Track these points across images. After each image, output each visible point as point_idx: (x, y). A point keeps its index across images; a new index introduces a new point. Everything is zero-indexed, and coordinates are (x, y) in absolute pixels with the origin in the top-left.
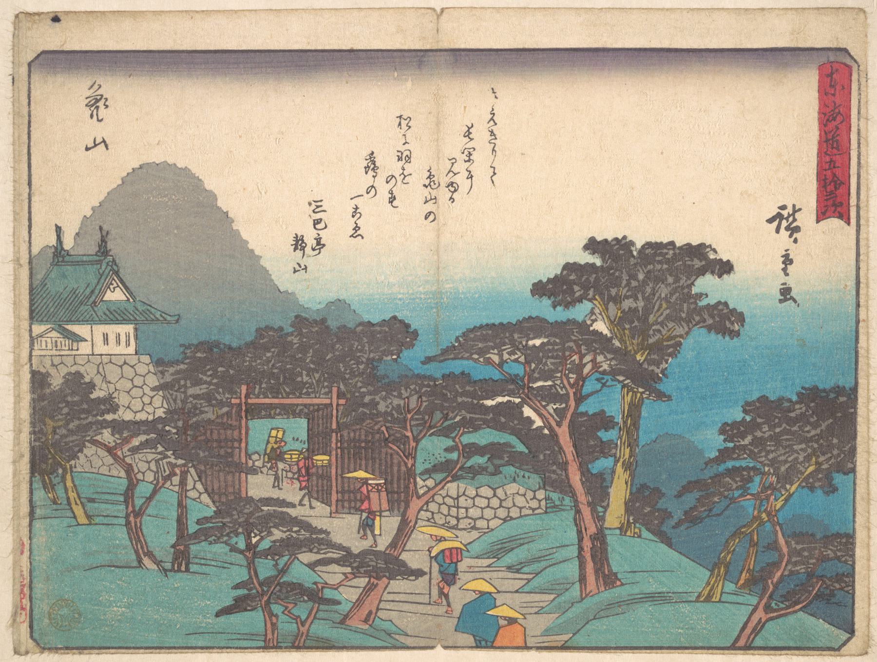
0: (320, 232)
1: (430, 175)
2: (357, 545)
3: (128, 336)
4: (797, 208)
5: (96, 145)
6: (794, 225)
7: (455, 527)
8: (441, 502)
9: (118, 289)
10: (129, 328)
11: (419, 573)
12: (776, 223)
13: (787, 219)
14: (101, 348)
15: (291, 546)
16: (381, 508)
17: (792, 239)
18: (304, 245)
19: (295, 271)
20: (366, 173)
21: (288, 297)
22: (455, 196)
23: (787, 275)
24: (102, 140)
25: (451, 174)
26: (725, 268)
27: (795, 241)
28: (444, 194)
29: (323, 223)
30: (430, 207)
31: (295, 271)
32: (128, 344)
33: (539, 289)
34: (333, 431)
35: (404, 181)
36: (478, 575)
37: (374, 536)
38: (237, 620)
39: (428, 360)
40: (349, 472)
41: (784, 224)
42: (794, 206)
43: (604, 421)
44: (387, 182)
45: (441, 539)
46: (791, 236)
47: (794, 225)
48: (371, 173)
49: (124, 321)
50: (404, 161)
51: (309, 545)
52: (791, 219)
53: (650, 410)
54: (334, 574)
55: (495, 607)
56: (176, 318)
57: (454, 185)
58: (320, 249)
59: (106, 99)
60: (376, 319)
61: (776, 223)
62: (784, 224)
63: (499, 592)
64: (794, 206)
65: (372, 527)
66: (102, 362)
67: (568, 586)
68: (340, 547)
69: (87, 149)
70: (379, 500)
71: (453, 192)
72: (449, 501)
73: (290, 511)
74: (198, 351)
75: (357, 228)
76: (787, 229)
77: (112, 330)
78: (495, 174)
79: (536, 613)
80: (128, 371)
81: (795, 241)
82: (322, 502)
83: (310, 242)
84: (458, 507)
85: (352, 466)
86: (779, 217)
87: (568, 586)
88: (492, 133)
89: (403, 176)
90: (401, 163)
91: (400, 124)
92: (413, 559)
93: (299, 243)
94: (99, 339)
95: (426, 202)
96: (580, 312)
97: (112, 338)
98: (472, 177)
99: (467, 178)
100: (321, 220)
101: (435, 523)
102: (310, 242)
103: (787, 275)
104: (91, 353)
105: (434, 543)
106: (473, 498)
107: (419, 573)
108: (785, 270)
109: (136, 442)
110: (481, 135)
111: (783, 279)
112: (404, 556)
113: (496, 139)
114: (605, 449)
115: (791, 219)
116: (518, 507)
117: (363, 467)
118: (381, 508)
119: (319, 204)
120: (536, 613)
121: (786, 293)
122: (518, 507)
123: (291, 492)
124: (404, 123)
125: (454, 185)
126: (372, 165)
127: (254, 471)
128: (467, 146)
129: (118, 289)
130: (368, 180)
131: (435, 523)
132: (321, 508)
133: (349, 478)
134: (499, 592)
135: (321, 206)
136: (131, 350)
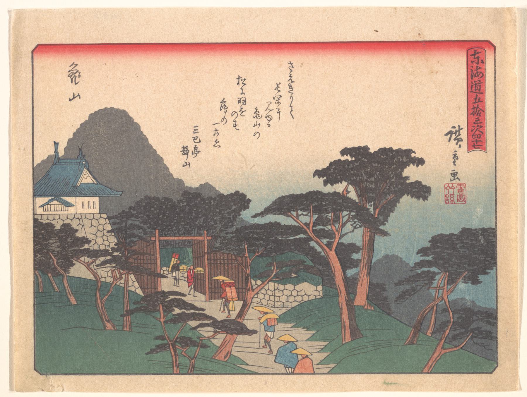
0: (197, 144)
1: (256, 111)
2: (220, 317)
3: (94, 203)
4: (461, 128)
5: (74, 98)
6: (459, 137)
7: (274, 306)
8: (265, 293)
9: (89, 177)
10: (96, 199)
11: (254, 332)
12: (449, 136)
13: (455, 133)
14: (80, 210)
15: (183, 318)
16: (276, 296)
17: (458, 145)
18: (188, 151)
19: (183, 166)
20: (221, 110)
21: (180, 182)
22: (271, 123)
23: (455, 165)
24: (78, 94)
25: (268, 111)
26: (420, 162)
27: (460, 146)
28: (263, 122)
29: (198, 139)
30: (256, 129)
31: (183, 166)
32: (94, 208)
33: (318, 173)
34: (205, 253)
35: (242, 115)
36: (286, 333)
37: (229, 311)
38: (156, 356)
39: (256, 216)
40: (214, 277)
41: (454, 136)
42: (459, 126)
43: (353, 248)
44: (232, 116)
45: (266, 313)
46: (457, 144)
47: (459, 137)
48: (223, 110)
49: (94, 195)
50: (242, 103)
51: (194, 317)
52: (457, 134)
53: (379, 240)
54: (207, 332)
55: (296, 349)
56: (121, 193)
57: (270, 117)
58: (196, 154)
59: (80, 73)
60: (225, 192)
61: (449, 136)
62: (454, 136)
63: (297, 341)
64: (459, 126)
65: (227, 306)
66: (81, 217)
67: (335, 337)
68: (210, 318)
69: (70, 100)
70: (231, 292)
71: (269, 121)
72: (270, 293)
73: (185, 298)
74: (296, 250)
75: (217, 141)
76: (455, 139)
77: (86, 200)
78: (292, 110)
79: (318, 352)
80: (95, 223)
81: (460, 146)
82: (201, 293)
83: (191, 149)
84: (275, 296)
85: (216, 273)
86: (450, 133)
87: (335, 337)
88: (290, 86)
89: (241, 112)
90: (240, 104)
91: (238, 83)
92: (250, 323)
93: (185, 151)
94: (79, 206)
95: (254, 126)
96: (340, 187)
97: (86, 205)
98: (280, 112)
99: (278, 113)
100: (197, 137)
101: (263, 305)
102: (191, 149)
103: (455, 165)
104: (75, 213)
105: (262, 315)
106: (282, 291)
107: (254, 332)
108: (454, 162)
109: (98, 262)
110: (284, 89)
111: (452, 167)
112: (245, 322)
113: (293, 90)
114: (355, 264)
115: (457, 134)
116: (294, 296)
117: (222, 273)
118: (276, 296)
119: (196, 128)
120: (318, 352)
121: (454, 175)
122: (294, 296)
123: (183, 287)
124: (241, 82)
125: (270, 117)
126: (223, 105)
127: (164, 277)
128: (277, 94)
129: (89, 177)
130: (222, 114)
131: (263, 305)
132: (201, 297)
133: (214, 279)
134: (297, 341)
135: (197, 130)
136: (96, 211)
